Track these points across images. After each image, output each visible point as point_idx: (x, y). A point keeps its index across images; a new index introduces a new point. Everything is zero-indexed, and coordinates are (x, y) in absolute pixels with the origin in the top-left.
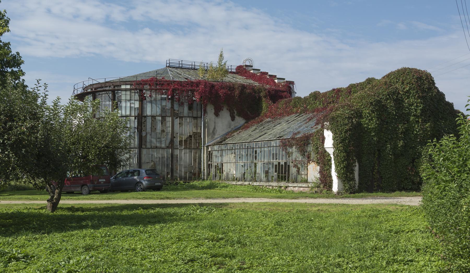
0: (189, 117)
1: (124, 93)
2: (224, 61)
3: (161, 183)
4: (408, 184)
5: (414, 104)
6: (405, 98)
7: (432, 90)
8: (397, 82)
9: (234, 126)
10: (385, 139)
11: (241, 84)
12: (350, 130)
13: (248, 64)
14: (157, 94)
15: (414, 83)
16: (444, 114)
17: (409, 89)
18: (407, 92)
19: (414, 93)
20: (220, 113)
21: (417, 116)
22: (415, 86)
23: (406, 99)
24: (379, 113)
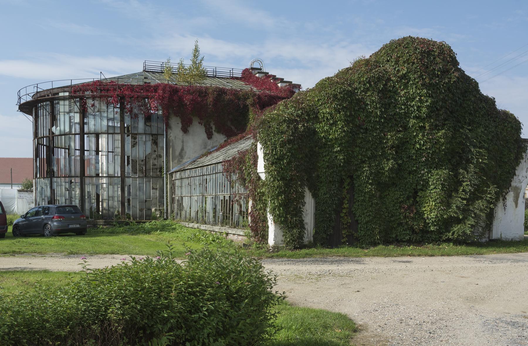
0: (145, 134)
1: (61, 102)
2: (200, 58)
3: (80, 224)
4: (404, 232)
5: (416, 97)
6: (400, 87)
7: (451, 74)
8: (388, 61)
9: (211, 146)
10: (360, 157)
11: (217, 88)
12: (289, 141)
13: (256, 66)
14: (102, 104)
15: (416, 61)
16: (476, 116)
17: (408, 72)
18: (404, 76)
19: (415, 79)
20: (189, 129)
21: (421, 119)
22: (417, 66)
23: (402, 90)
24: (348, 114)
